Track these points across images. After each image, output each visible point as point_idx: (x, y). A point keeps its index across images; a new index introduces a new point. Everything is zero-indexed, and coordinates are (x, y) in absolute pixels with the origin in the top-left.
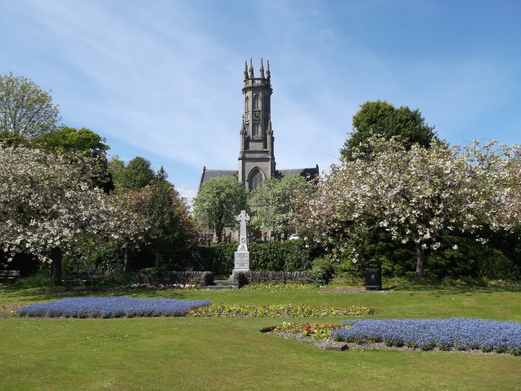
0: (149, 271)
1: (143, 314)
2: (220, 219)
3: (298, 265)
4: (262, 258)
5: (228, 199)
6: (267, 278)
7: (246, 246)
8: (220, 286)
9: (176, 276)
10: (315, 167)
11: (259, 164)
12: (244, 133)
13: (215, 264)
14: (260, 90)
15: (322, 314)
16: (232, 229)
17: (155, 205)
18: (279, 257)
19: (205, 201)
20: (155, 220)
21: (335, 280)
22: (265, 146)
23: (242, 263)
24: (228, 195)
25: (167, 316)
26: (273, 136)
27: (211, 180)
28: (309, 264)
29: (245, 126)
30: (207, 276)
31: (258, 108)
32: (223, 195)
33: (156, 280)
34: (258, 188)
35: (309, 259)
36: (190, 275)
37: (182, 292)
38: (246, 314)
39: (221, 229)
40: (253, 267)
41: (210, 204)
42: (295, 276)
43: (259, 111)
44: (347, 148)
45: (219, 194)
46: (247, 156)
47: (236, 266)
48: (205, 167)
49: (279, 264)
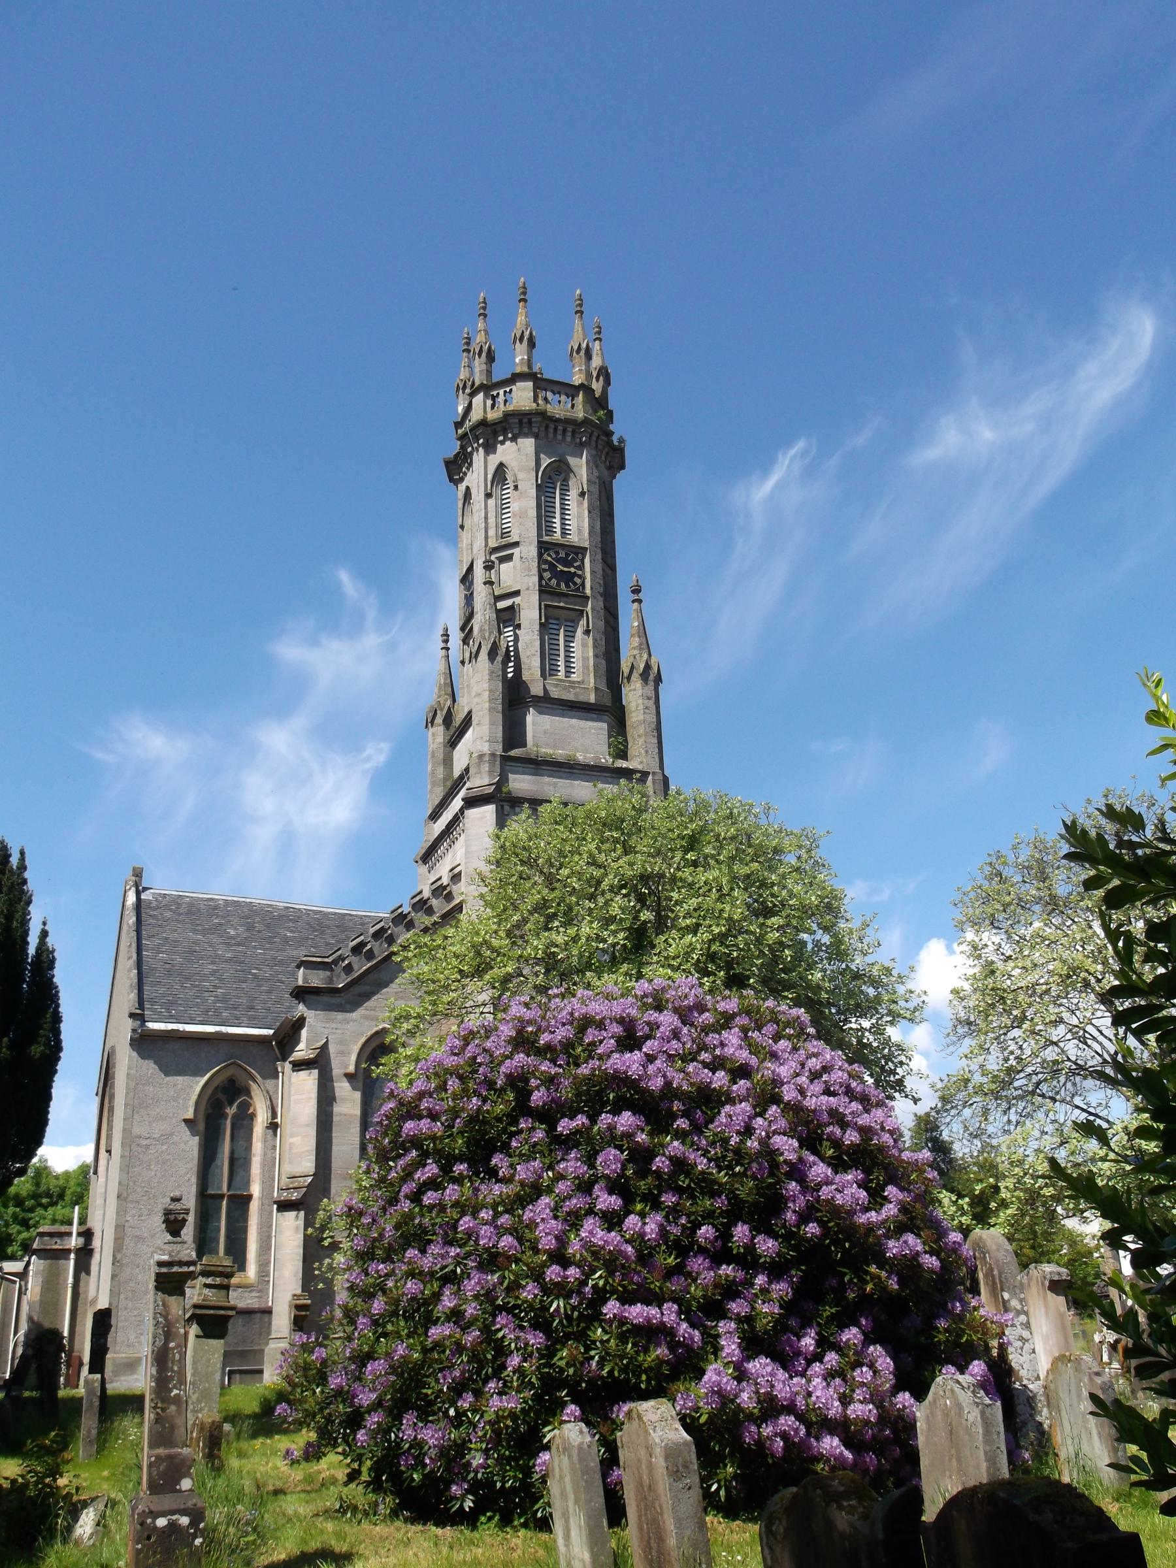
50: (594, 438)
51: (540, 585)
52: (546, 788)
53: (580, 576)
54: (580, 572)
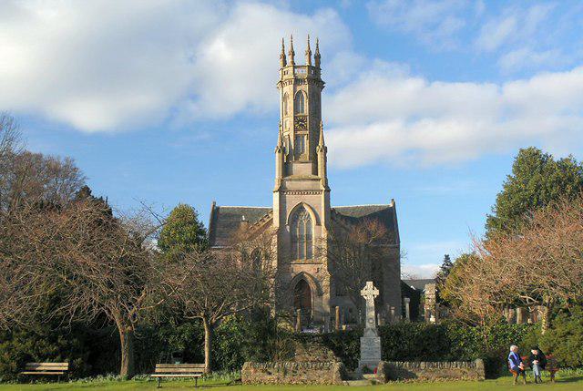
10: (391, 205)
22: (315, 172)
31: (303, 111)
47: (363, 355)
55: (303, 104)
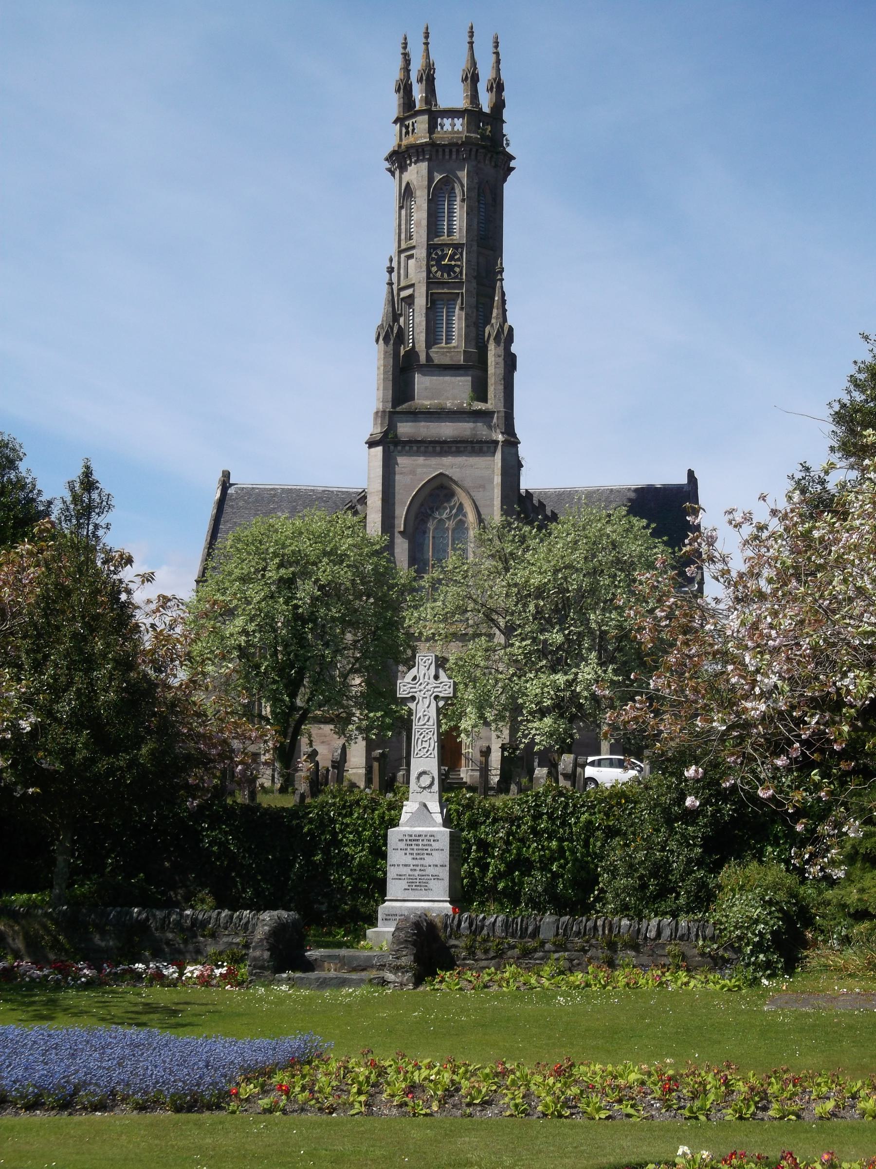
0: (32, 906)
1: (38, 1096)
2: (293, 688)
3: (655, 888)
4: (502, 858)
5: (328, 606)
6: (532, 944)
7: (434, 806)
8: (333, 974)
9: (142, 927)
10: (684, 480)
11: (451, 466)
12: (392, 335)
13: (310, 880)
14: (462, 160)
15: (819, 1109)
16: (341, 732)
17: (58, 628)
18: (573, 852)
19: (230, 613)
20: (57, 690)
21: (821, 956)
23: (417, 875)
24: (329, 592)
25: (141, 1108)
26: (514, 349)
27: (255, 526)
28: (702, 885)
29: (398, 306)
30: (278, 932)
31: (450, 233)
32: (305, 591)
33: (56, 945)
34: (451, 561)
35: (700, 863)
36: (204, 924)
37: (175, 998)
38: (486, 1104)
39: (297, 732)
40: (461, 897)
41: (251, 627)
42: (652, 934)
43: (457, 246)
44: (859, 397)
45: (288, 583)
46: (405, 429)
47: (394, 888)
48: (226, 475)
49: (575, 883)
50: (473, 153)
51: (428, 277)
52: (422, 430)
53: (458, 266)
54: (459, 263)
55: (451, 212)
